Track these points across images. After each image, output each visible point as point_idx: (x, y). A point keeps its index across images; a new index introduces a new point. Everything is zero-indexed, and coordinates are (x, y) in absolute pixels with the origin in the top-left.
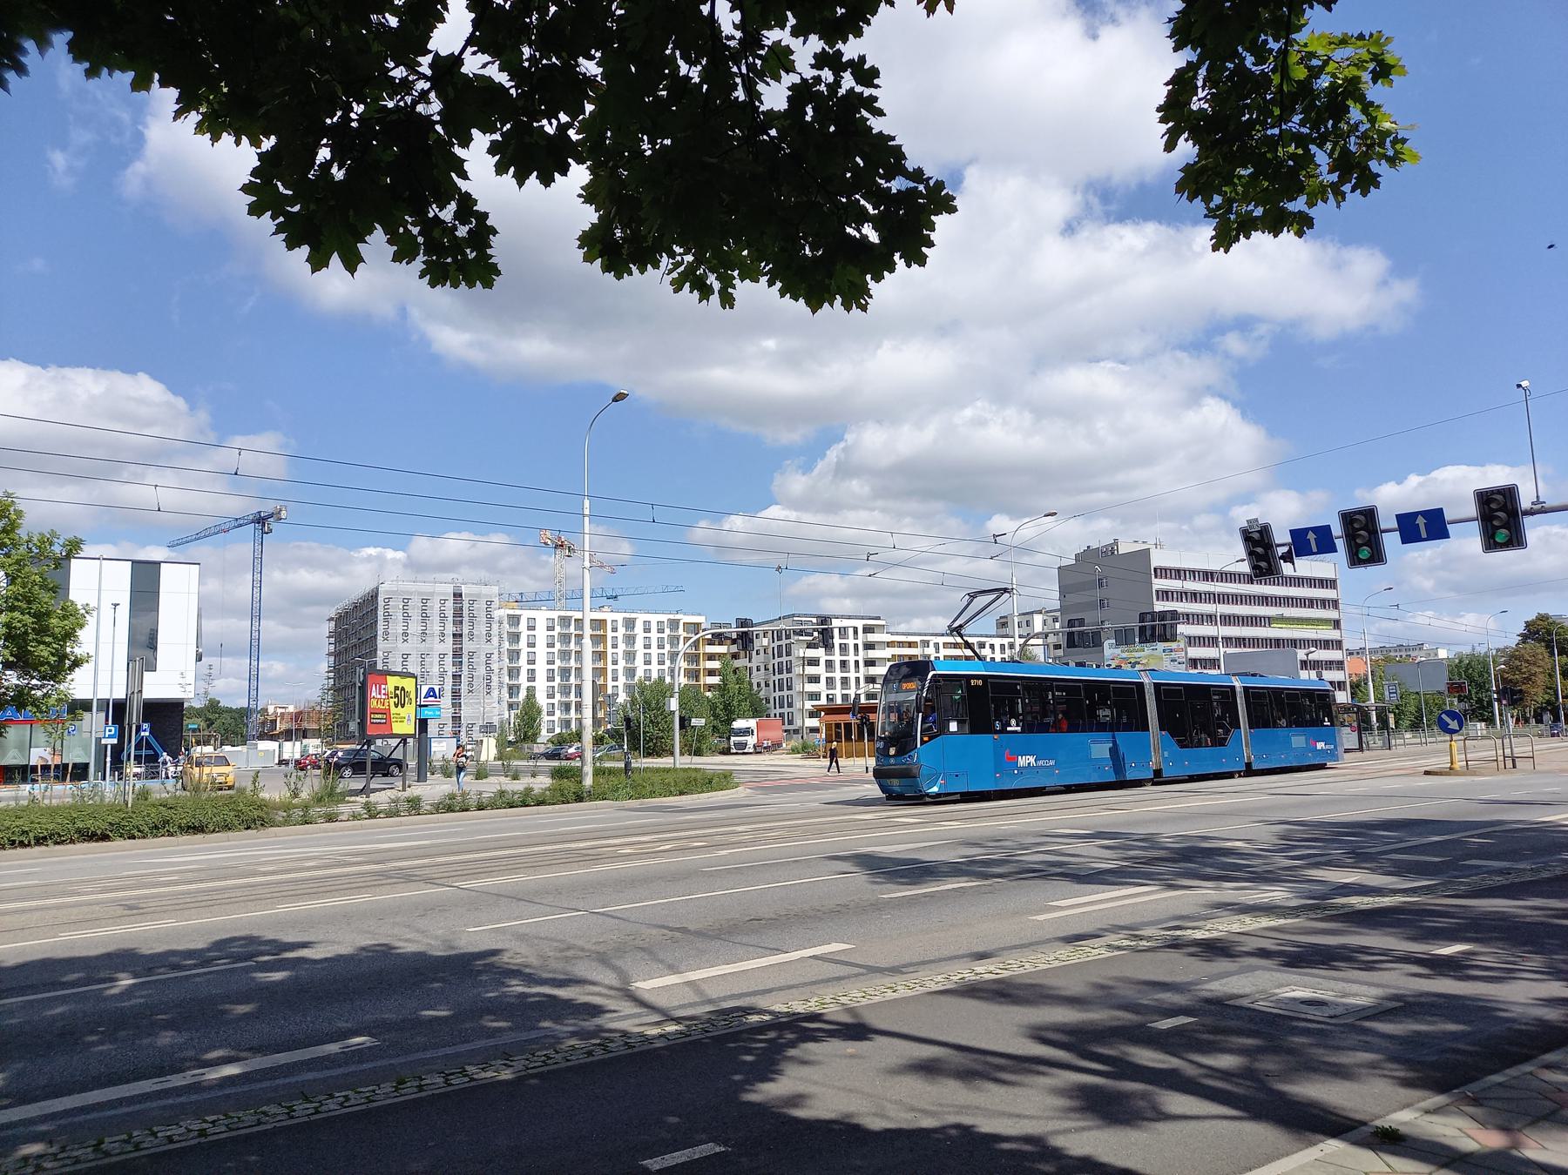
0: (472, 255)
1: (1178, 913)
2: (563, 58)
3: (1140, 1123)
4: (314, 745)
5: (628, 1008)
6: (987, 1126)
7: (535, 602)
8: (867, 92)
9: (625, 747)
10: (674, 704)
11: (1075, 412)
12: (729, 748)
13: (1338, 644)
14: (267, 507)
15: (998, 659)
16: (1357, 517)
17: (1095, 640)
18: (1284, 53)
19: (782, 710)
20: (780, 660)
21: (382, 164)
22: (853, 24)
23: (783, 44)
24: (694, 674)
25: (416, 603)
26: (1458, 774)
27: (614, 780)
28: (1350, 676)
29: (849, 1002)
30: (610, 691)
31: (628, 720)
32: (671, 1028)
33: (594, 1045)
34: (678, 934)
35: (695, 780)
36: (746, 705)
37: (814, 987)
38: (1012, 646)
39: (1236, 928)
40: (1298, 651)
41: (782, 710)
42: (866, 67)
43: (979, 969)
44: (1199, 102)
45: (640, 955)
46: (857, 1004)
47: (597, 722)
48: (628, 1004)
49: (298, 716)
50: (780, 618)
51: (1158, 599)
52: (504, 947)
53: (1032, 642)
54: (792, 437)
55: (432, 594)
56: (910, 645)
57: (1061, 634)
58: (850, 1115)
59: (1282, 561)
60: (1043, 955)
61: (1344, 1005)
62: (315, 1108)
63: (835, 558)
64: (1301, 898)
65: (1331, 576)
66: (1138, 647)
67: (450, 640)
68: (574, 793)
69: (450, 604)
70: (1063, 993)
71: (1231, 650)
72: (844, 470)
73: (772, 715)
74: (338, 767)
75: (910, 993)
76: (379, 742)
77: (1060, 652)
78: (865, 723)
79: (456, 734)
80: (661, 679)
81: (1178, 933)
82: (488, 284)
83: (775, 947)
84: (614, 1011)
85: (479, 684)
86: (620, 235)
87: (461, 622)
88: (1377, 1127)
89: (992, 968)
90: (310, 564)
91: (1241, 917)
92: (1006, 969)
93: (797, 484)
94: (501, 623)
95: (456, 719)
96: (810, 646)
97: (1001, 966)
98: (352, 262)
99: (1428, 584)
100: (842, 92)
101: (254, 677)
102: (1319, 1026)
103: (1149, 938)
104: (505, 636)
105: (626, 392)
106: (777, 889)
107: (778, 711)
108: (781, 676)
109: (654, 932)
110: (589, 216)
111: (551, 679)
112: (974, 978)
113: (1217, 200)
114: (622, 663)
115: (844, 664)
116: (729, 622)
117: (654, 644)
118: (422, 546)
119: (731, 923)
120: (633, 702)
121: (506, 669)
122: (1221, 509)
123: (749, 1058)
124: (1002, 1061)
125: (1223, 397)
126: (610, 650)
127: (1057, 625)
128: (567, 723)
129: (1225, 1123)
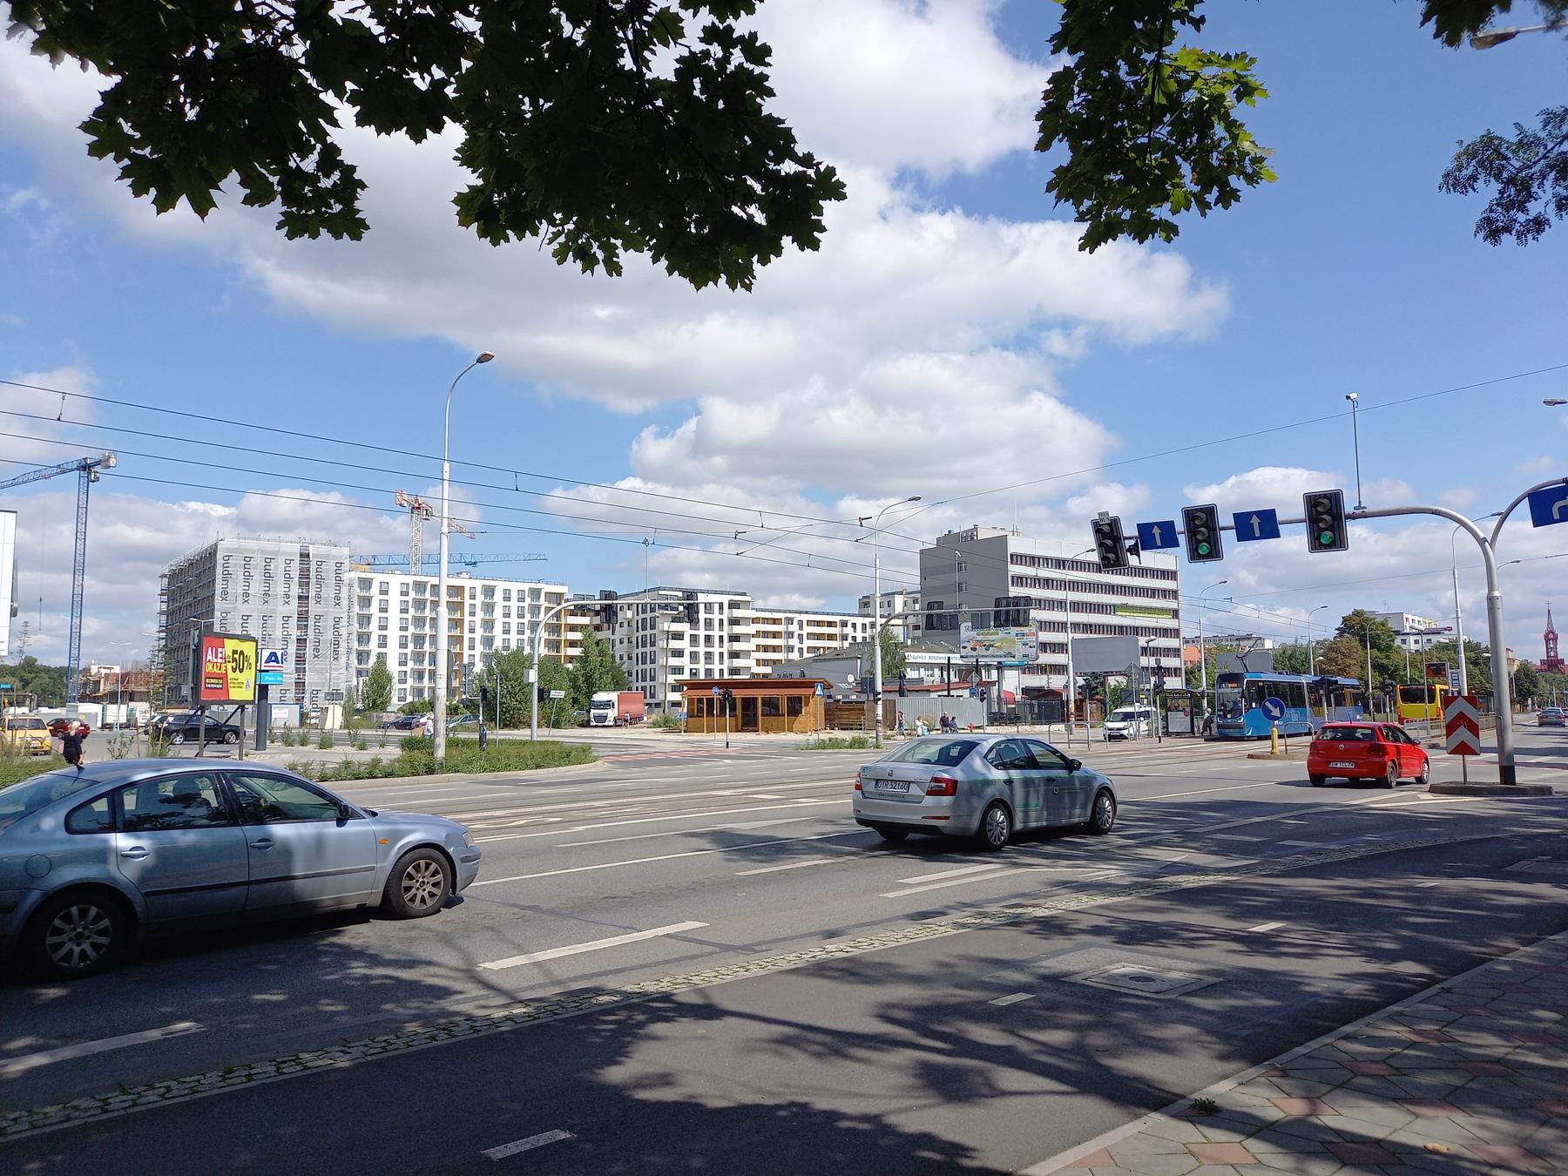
0: (337, 208)
1: (1020, 890)
2: (438, 9)
4: (142, 711)
7: (390, 565)
8: (758, 70)
9: (481, 718)
10: (533, 676)
12: (589, 721)
14: (93, 455)
15: (859, 640)
19: (644, 684)
20: (644, 633)
21: (239, 104)
24: (554, 645)
25: (258, 561)
27: (468, 752)
29: (701, 982)
30: (466, 661)
31: (484, 691)
32: (518, 1010)
34: (529, 913)
35: (553, 754)
36: (607, 678)
37: (667, 966)
38: (873, 625)
41: (644, 684)
42: (757, 44)
43: (830, 947)
45: (489, 934)
46: (710, 984)
47: (451, 692)
49: (124, 677)
50: (645, 591)
53: (893, 622)
56: (775, 621)
60: (892, 933)
62: (134, 1100)
66: (993, 630)
67: (295, 602)
68: (425, 765)
69: (296, 565)
73: (634, 688)
74: (168, 733)
76: (214, 708)
77: (919, 633)
78: (728, 699)
79: (300, 701)
80: (520, 649)
81: (1020, 910)
83: (629, 925)
85: (327, 650)
90: (132, 522)
92: (856, 947)
93: (654, 449)
94: (351, 586)
95: (300, 685)
96: (675, 620)
98: (202, 206)
100: (731, 68)
101: (75, 636)
104: (355, 600)
105: (491, 353)
106: (627, 867)
107: (640, 684)
108: (644, 650)
109: (505, 910)
111: (403, 645)
112: (825, 956)
114: (479, 632)
115: (708, 639)
116: (593, 594)
117: (514, 613)
118: (254, 502)
120: (490, 672)
121: (355, 634)
126: (467, 618)
127: (917, 607)
128: (420, 692)
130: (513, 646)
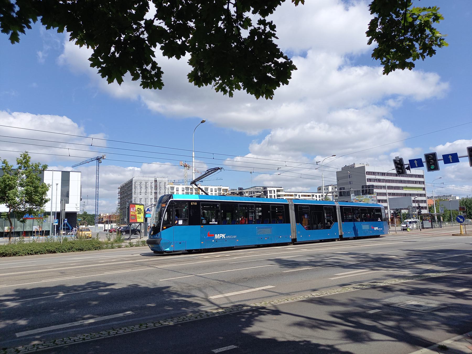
0: (156, 80)
3: (364, 342)
5: (208, 304)
6: (314, 341)
8: (273, 32)
11: (342, 124)
13: (424, 195)
16: (430, 156)
17: (348, 194)
18: (405, 14)
22: (270, 10)
23: (249, 18)
26: (463, 235)
28: (428, 205)
29: (274, 304)
32: (220, 310)
33: (198, 315)
34: (222, 282)
37: (263, 299)
38: (322, 196)
39: (393, 282)
40: (412, 197)
43: (313, 294)
44: (379, 29)
46: (276, 304)
48: (207, 303)
50: (251, 188)
51: (367, 181)
52: (170, 286)
53: (328, 194)
54: (255, 133)
56: (291, 195)
57: (337, 192)
58: (275, 337)
59: (406, 170)
60: (333, 290)
61: (428, 306)
63: (268, 170)
64: (413, 273)
65: (422, 174)
66: (361, 196)
67: (153, 194)
69: (153, 184)
70: (339, 302)
71: (390, 197)
72: (271, 143)
75: (292, 301)
77: (337, 198)
81: (375, 284)
82: (160, 88)
84: (204, 305)
86: (200, 74)
87: (157, 189)
88: (439, 345)
89: (317, 294)
91: (395, 279)
97: (320, 293)
99: (453, 176)
102: (418, 313)
103: (366, 285)
105: (205, 120)
109: (215, 281)
110: (191, 69)
113: (385, 59)
119: (238, 279)
122: (387, 153)
123: (243, 320)
124: (323, 323)
125: (388, 119)
127: (336, 189)
129: (391, 342)
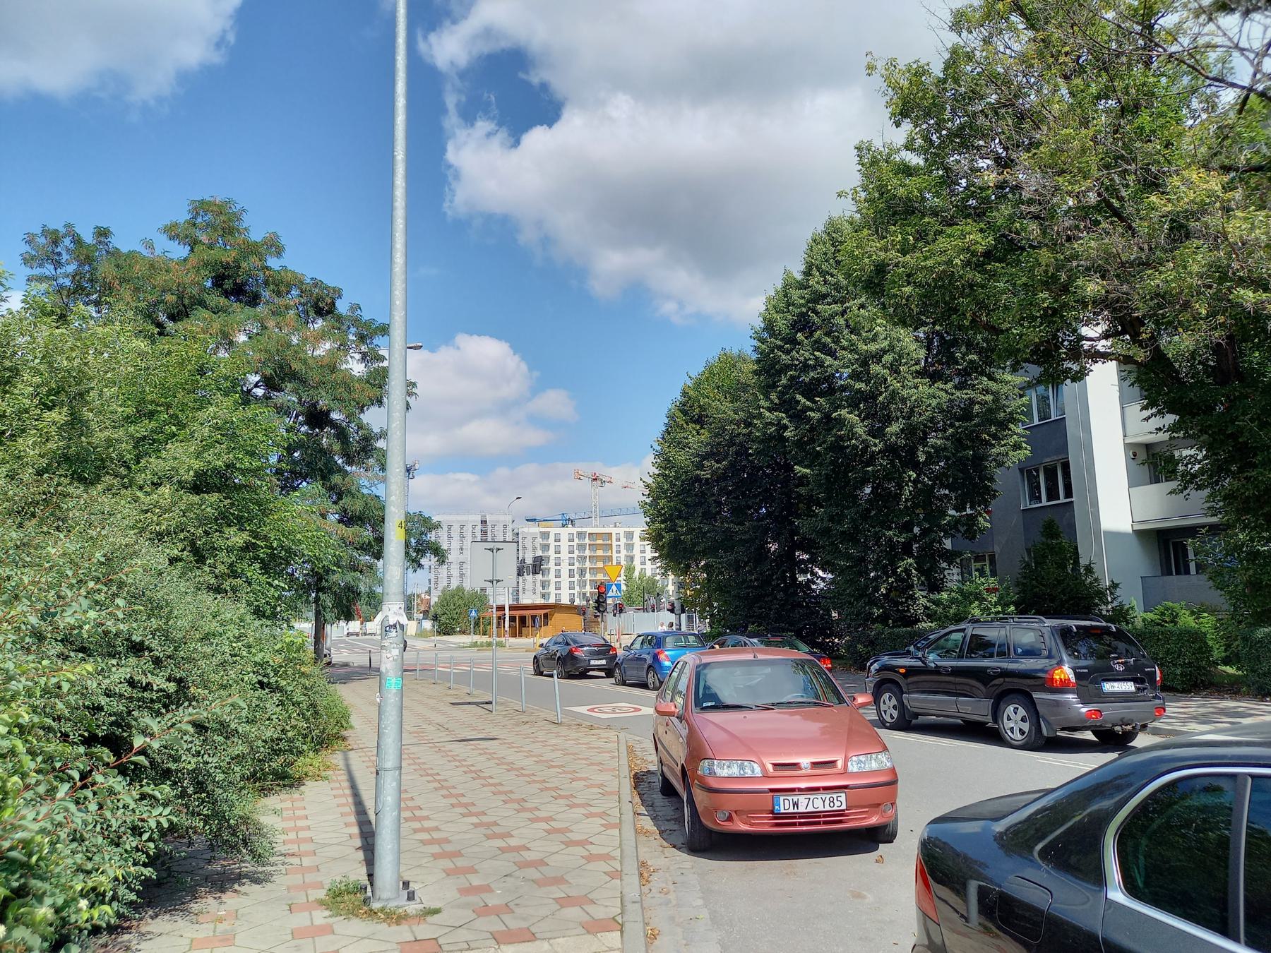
25: (456, 528)
55: (467, 521)
111: (571, 576)
130: (649, 573)
